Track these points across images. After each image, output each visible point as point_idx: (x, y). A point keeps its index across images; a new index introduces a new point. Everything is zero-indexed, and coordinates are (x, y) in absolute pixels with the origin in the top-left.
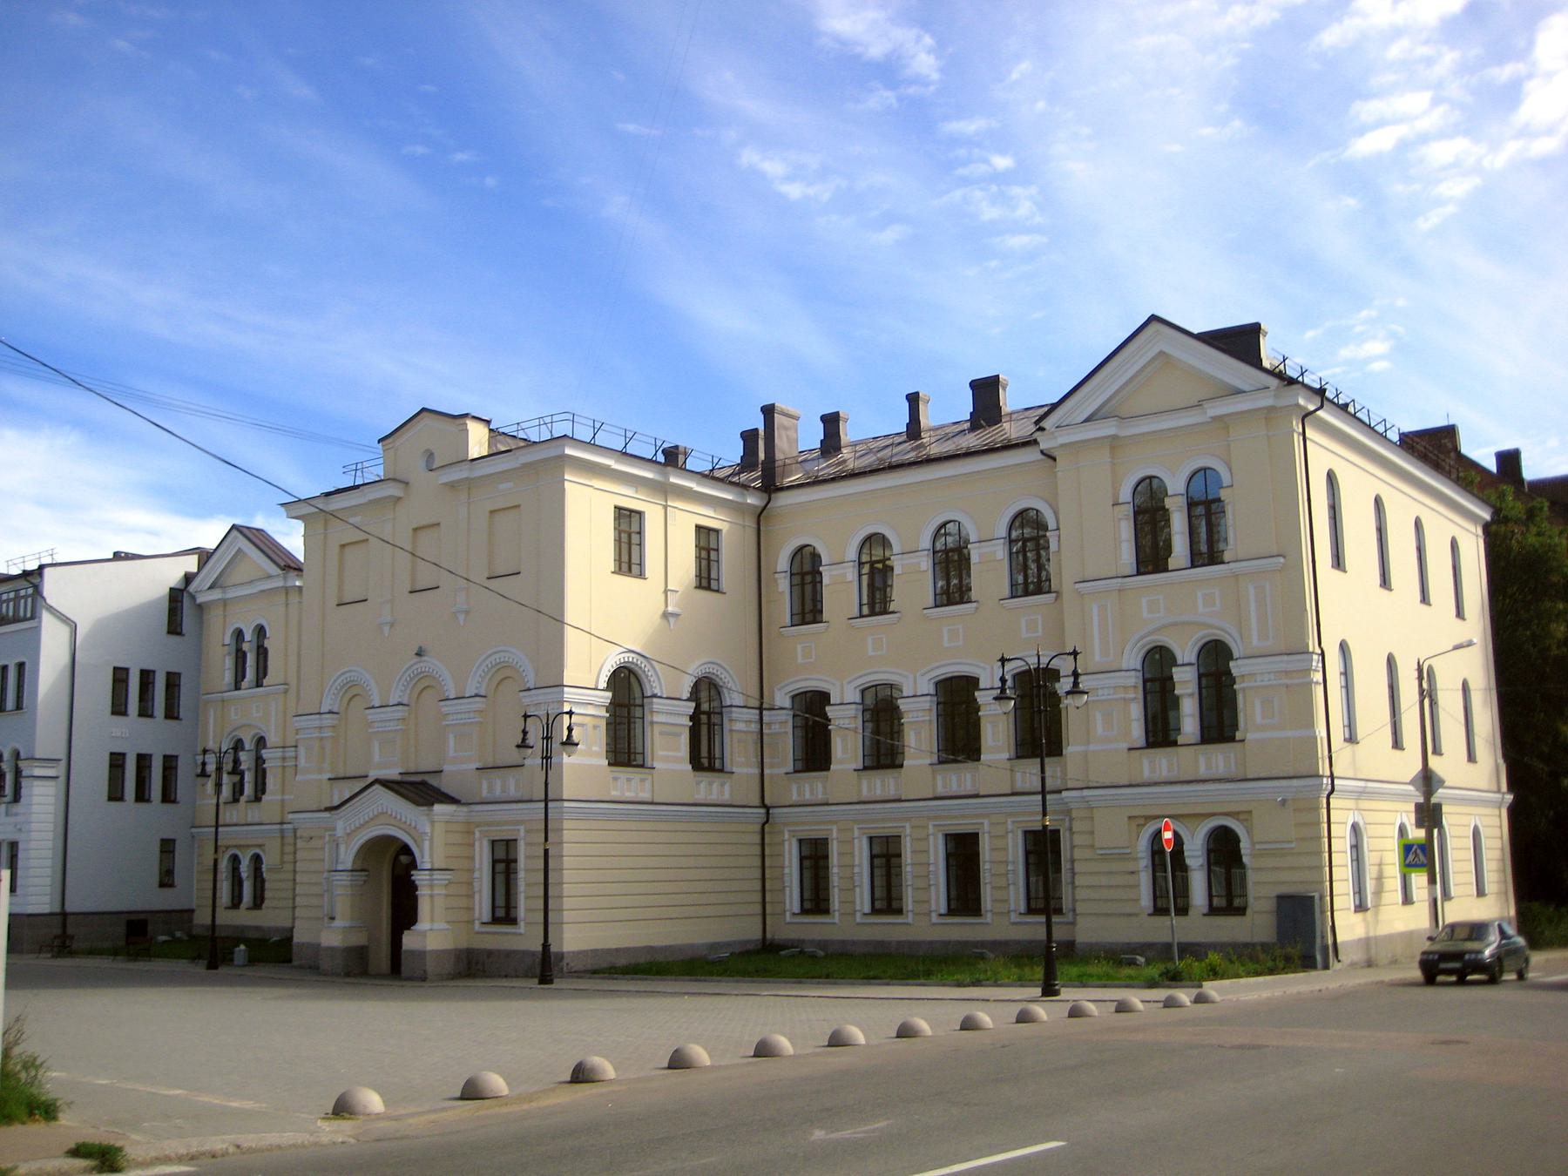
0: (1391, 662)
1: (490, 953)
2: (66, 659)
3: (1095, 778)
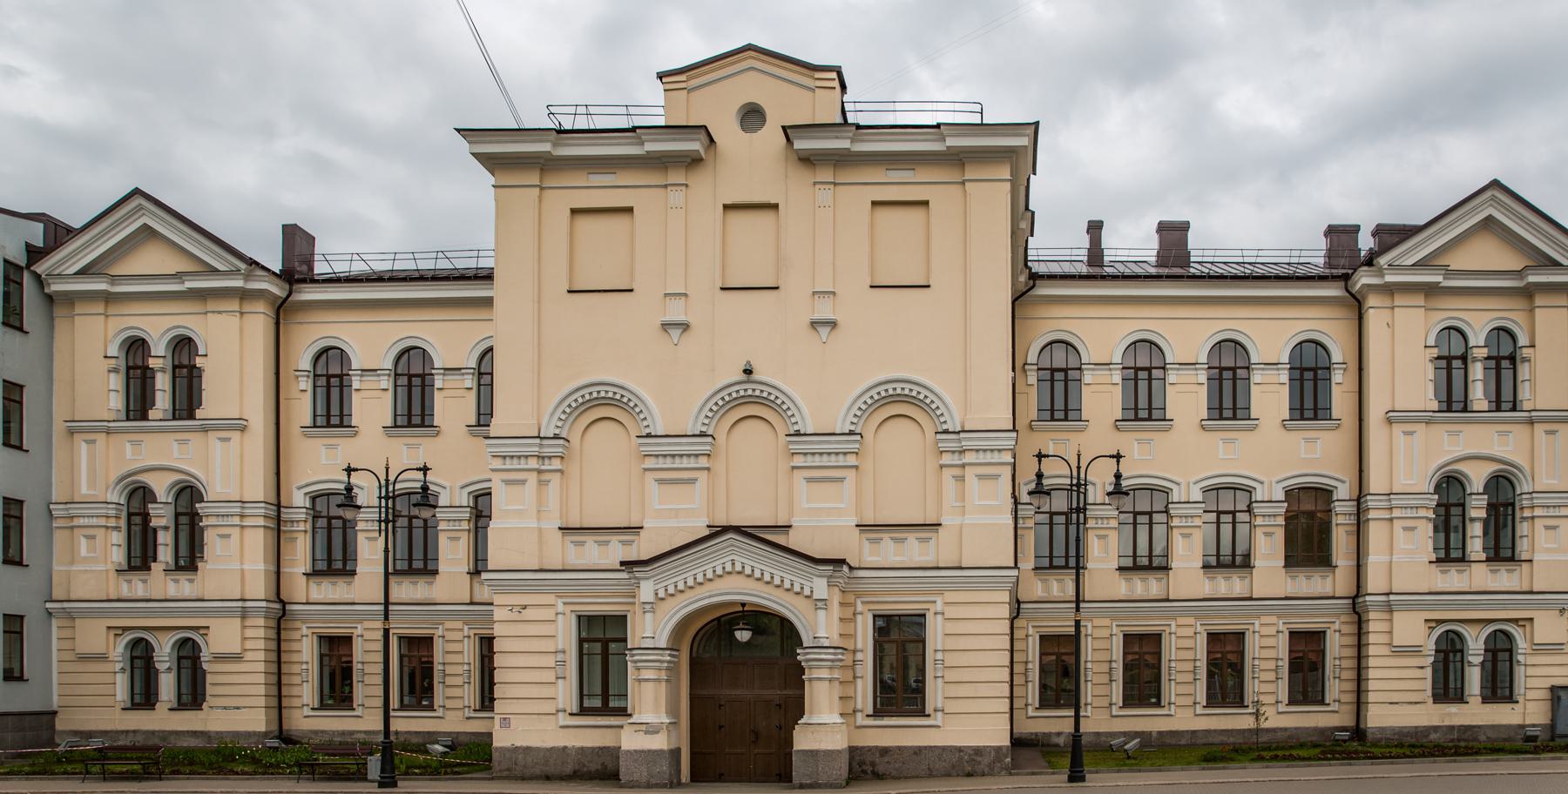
1: (885, 751)
2: (56, 335)
3: (73, 597)
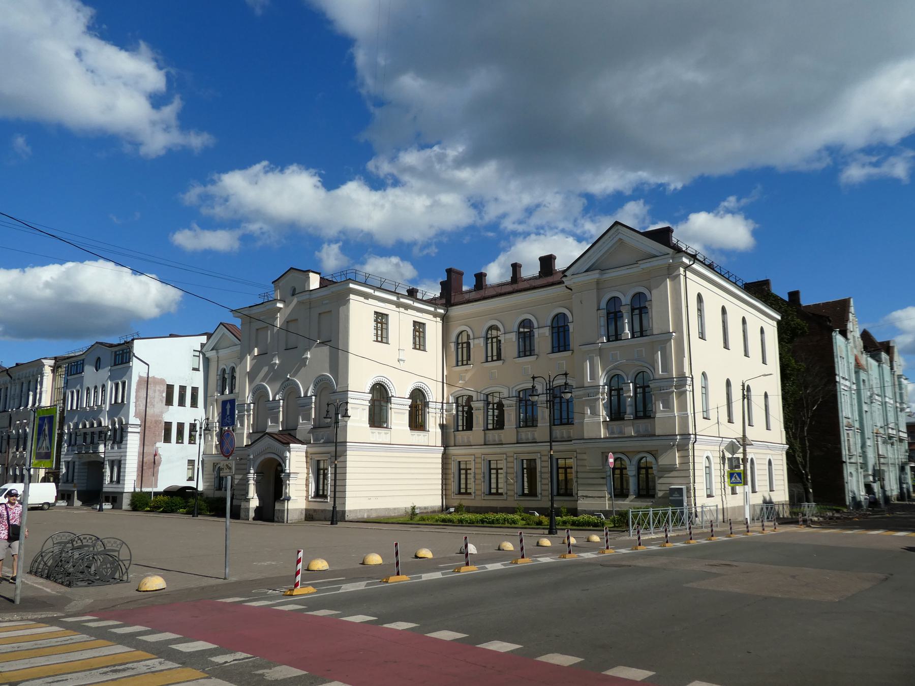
0: (728, 383)
